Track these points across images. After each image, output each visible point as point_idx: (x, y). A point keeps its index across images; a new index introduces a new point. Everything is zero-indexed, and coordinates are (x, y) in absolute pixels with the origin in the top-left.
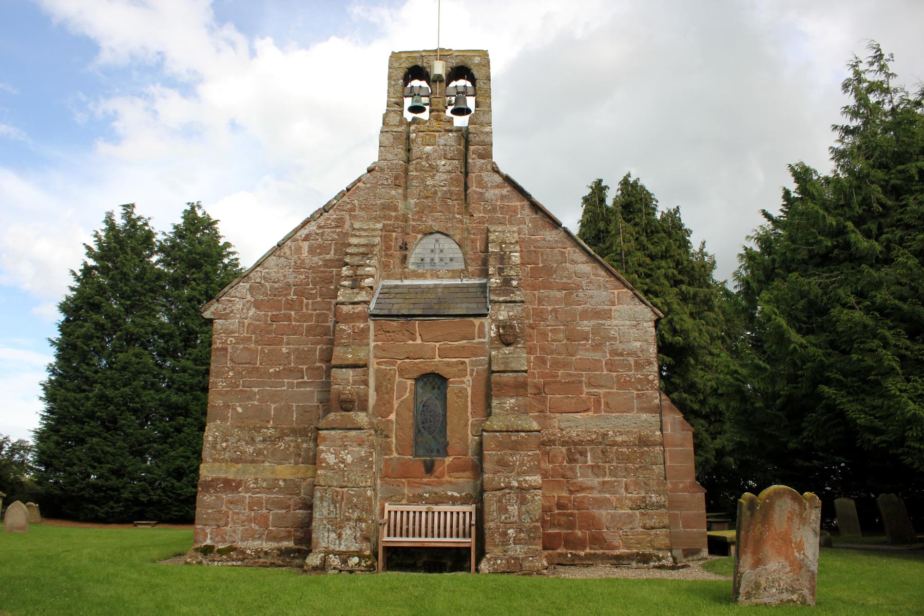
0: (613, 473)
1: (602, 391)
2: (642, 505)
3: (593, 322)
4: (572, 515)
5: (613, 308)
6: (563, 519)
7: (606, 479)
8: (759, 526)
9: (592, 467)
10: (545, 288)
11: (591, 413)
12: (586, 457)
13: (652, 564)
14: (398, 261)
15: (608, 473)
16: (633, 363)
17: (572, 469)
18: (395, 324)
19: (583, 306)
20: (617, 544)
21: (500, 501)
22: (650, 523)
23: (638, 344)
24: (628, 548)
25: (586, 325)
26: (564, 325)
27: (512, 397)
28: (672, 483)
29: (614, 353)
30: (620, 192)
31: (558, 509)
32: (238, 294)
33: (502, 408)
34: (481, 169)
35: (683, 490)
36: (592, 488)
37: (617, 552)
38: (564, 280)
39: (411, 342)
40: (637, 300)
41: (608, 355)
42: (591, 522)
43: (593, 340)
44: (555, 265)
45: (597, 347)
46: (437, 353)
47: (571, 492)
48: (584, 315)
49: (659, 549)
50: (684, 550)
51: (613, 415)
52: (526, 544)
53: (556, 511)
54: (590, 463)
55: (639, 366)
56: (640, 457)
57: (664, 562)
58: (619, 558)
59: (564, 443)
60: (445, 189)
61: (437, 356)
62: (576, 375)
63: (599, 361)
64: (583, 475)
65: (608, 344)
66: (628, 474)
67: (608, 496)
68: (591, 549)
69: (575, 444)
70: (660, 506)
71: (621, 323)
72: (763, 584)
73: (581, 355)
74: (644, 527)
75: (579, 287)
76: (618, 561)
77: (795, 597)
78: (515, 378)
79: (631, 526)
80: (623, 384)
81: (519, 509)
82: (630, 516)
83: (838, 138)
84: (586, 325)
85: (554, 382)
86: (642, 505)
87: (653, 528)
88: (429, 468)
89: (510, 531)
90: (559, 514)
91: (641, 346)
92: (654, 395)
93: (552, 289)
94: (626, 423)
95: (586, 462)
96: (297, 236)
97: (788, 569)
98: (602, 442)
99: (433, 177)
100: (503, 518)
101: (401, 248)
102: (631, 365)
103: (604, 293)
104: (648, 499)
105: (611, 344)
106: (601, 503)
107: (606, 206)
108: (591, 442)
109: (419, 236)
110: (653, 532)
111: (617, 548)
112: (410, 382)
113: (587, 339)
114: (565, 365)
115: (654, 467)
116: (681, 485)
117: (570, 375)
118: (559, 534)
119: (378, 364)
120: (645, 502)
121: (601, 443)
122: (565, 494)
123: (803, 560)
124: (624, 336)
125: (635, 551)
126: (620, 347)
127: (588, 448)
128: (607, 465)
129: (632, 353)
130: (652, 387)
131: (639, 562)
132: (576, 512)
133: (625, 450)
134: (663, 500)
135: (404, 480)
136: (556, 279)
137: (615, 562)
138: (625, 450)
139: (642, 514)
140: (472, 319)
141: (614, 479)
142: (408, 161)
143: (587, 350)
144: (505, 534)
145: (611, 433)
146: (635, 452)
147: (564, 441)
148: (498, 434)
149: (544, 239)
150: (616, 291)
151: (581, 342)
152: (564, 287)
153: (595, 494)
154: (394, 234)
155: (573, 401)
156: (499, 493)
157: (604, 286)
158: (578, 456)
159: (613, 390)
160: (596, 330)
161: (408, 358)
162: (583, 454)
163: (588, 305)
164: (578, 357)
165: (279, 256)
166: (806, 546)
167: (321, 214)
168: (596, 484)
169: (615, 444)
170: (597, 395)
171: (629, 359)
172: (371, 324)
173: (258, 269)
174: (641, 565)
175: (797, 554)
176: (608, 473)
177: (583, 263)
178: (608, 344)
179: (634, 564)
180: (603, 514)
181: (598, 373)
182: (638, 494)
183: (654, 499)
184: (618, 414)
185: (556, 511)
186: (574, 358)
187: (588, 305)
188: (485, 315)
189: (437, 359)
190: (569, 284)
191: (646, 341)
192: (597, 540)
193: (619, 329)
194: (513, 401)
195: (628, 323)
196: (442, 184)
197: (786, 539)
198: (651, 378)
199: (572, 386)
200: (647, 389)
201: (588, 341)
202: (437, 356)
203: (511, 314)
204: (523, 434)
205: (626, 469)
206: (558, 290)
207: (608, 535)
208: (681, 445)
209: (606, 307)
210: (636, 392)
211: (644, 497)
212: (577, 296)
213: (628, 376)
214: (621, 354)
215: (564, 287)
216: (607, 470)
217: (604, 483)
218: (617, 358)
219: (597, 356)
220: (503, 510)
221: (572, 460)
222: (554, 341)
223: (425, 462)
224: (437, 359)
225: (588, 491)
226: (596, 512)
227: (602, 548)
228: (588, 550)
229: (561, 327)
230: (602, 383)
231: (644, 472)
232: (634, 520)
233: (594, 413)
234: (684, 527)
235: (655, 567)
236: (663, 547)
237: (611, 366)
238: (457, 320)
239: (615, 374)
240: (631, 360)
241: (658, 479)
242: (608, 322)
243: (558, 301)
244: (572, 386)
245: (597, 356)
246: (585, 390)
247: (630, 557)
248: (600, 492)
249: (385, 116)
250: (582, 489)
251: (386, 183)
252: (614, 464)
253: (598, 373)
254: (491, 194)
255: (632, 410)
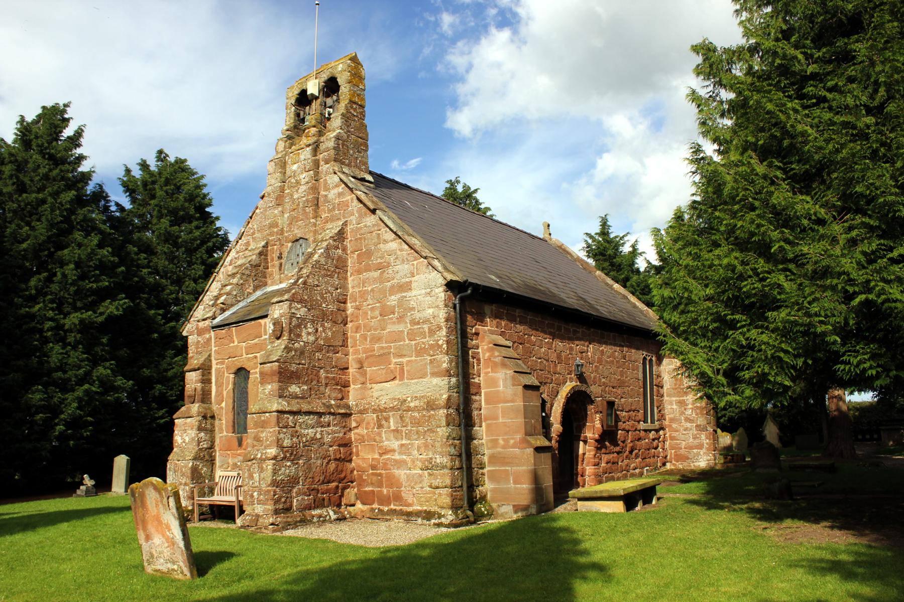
0: (408, 437)
1: (404, 360)
2: (429, 466)
3: (399, 296)
4: (380, 475)
5: (413, 279)
6: (375, 478)
7: (404, 442)
8: (141, 509)
9: (393, 431)
10: (366, 271)
11: (397, 382)
12: (389, 422)
13: (433, 521)
14: (277, 269)
17: (379, 434)
18: (223, 331)
20: (411, 502)
21: (249, 470)
22: (436, 483)
23: (431, 311)
24: (421, 505)
25: (393, 300)
26: (380, 302)
28: (504, 440)
29: (414, 322)
33: (264, 393)
34: (327, 173)
35: (514, 446)
36: (394, 451)
37: (410, 509)
39: (232, 345)
40: (430, 267)
41: (409, 326)
42: (393, 481)
43: (398, 312)
45: (401, 319)
47: (381, 455)
48: (394, 290)
49: (442, 508)
50: (514, 506)
51: (413, 381)
52: (263, 504)
53: (371, 471)
54: (393, 428)
55: (432, 332)
56: (428, 421)
57: (443, 520)
58: (409, 514)
59: (374, 411)
60: (304, 199)
61: (244, 354)
62: (386, 348)
63: (402, 332)
64: (387, 439)
65: (409, 314)
66: (419, 437)
67: (404, 457)
68: (394, 505)
69: (381, 411)
70: (443, 467)
71: (419, 292)
72: (156, 555)
73: (391, 328)
74: (431, 487)
76: (409, 516)
77: (175, 567)
78: (271, 367)
79: (421, 485)
80: (420, 352)
82: (421, 476)
84: (393, 300)
85: (371, 356)
86: (429, 466)
87: (437, 488)
88: (240, 444)
89: (255, 494)
90: (373, 474)
92: (443, 360)
93: (370, 271)
94: (421, 389)
97: (166, 545)
98: (401, 407)
101: (279, 257)
102: (425, 333)
103: (406, 266)
104: (434, 460)
105: (412, 315)
106: (400, 464)
107: (737, 97)
110: (437, 491)
112: (232, 376)
113: (393, 313)
114: (379, 339)
115: (438, 430)
116: (512, 442)
117: (382, 348)
118: (373, 491)
120: (431, 463)
122: (377, 456)
123: (173, 538)
124: (420, 305)
125: (425, 508)
126: (417, 316)
127: (391, 414)
128: (404, 429)
129: (427, 321)
130: (441, 352)
131: (423, 519)
132: (383, 472)
133: (416, 414)
134: (445, 461)
135: (229, 452)
136: (375, 261)
137: (406, 518)
138: (416, 414)
139: (430, 475)
140: (260, 321)
141: (409, 442)
143: (394, 323)
144: (252, 496)
145: (409, 399)
146: (424, 416)
147: (374, 409)
148: (254, 415)
149: (365, 226)
150: (415, 263)
151: (390, 316)
152: (379, 267)
153: (397, 457)
154: (275, 247)
155: (384, 372)
156: (250, 463)
158: (384, 422)
159: (413, 358)
160: (401, 302)
161: (229, 358)
162: (387, 419)
163: (396, 281)
164: (388, 330)
166: (172, 527)
167: (237, 242)
168: (396, 448)
169: (409, 409)
170: (401, 364)
171: (424, 326)
172: (212, 333)
174: (425, 521)
175: (168, 533)
177: (392, 241)
178: (409, 314)
179: (420, 521)
180: (401, 474)
181: (402, 343)
182: (427, 455)
183: (438, 461)
184: (416, 381)
185: (371, 471)
187: (396, 281)
188: (266, 316)
189: (245, 356)
190: (382, 263)
191: (437, 307)
192: (398, 498)
193: (417, 299)
195: (423, 291)
197: (158, 519)
198: (440, 342)
199: (383, 358)
200: (438, 354)
202: (244, 354)
203: (281, 311)
204: (267, 414)
205: (417, 432)
206: (375, 270)
207: (407, 496)
208: (512, 401)
209: (407, 280)
210: (429, 358)
211: (431, 459)
213: (423, 343)
214: (418, 323)
215: (379, 267)
216: (404, 434)
217: (402, 445)
218: (416, 327)
219: (401, 327)
221: (380, 426)
222: (372, 318)
223: (238, 437)
224: (245, 356)
225: (392, 453)
226: (396, 472)
227: (401, 505)
228: (392, 507)
229: (377, 305)
230: (404, 353)
231: (431, 435)
232: (423, 480)
233: (400, 381)
234: (515, 482)
235: (435, 524)
236: (445, 505)
237: (412, 336)
238: (253, 322)
239: (413, 342)
240: (426, 327)
241: (442, 441)
242: (408, 294)
243: (375, 280)
244: (383, 358)
245: (401, 327)
247: (418, 514)
248: (400, 453)
250: (387, 452)
252: (409, 428)
254: (332, 194)
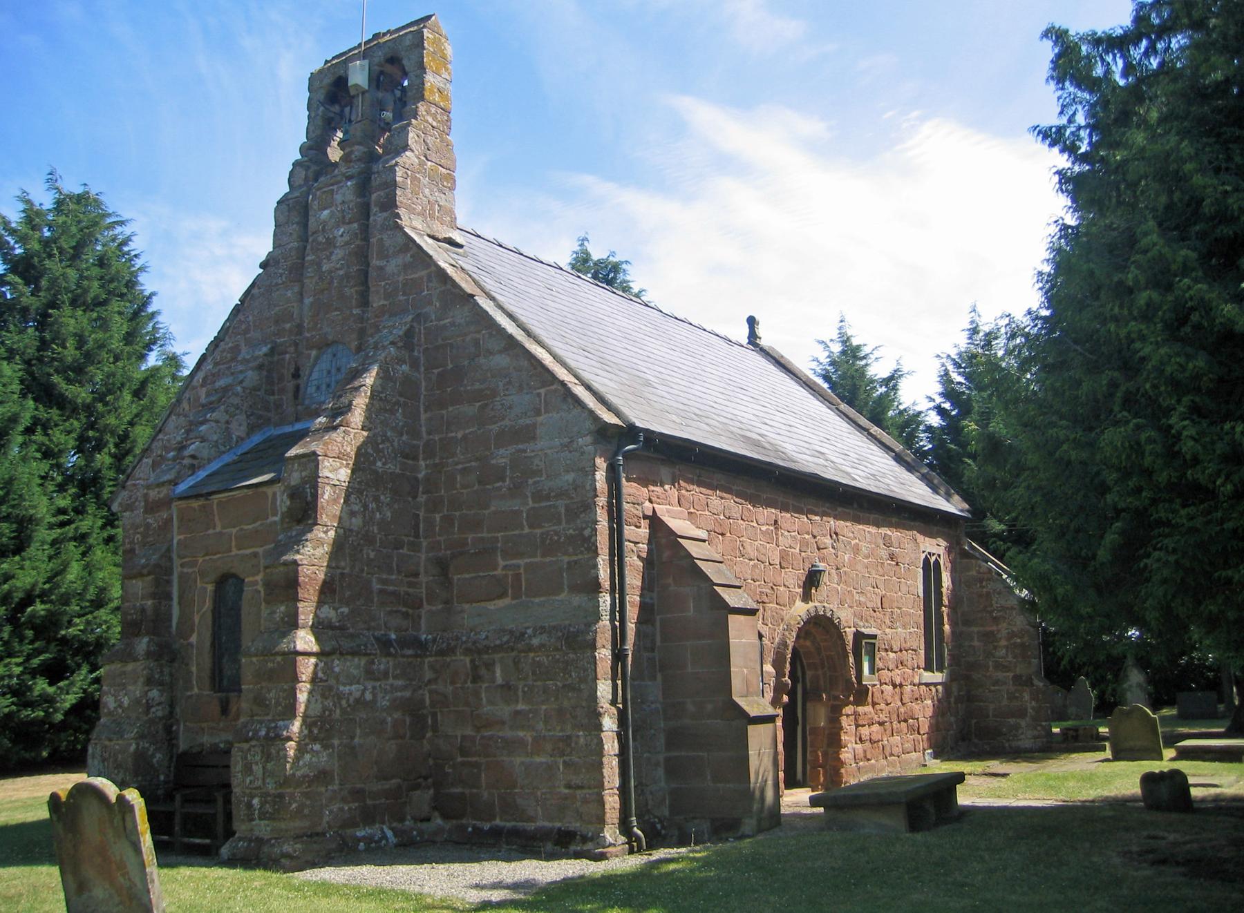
1: (521, 562)
3: (511, 449)
5: (540, 419)
12: (494, 672)
15: (521, 698)
16: (563, 510)
17: (477, 694)
19: (499, 424)
22: (576, 780)
25: (502, 457)
27: (282, 602)
29: (538, 496)
30: (1120, 32)
31: (462, 756)
32: (142, 475)
37: (531, 826)
38: (477, 386)
41: (530, 502)
44: (466, 363)
46: (233, 543)
59: (468, 651)
60: (341, 272)
64: (490, 702)
65: (530, 481)
69: (479, 652)
75: (495, 393)
81: (264, 768)
83: (144, 274)
87: (581, 788)
91: (574, 481)
95: (493, 680)
96: (195, 383)
99: (328, 258)
100: (248, 781)
103: (527, 398)
108: (499, 648)
109: (314, 353)
111: (531, 819)
116: (710, 707)
119: (182, 565)
121: (513, 649)
122: (469, 732)
127: (497, 656)
129: (562, 494)
140: (264, 489)
142: (304, 239)
150: (542, 391)
157: (528, 384)
162: (490, 666)
163: (507, 422)
165: (179, 415)
173: (160, 436)
176: (521, 698)
181: (517, 532)
185: (459, 759)
186: (486, 512)
187: (507, 422)
194: (283, 608)
196: (338, 266)
201: (504, 481)
209: (528, 422)
212: (492, 409)
213: (557, 533)
217: (517, 713)
219: (515, 505)
220: (248, 769)
233: (513, 598)
245: (515, 505)
246: (502, 563)
249: (291, 173)
250: (489, 725)
251: (280, 282)
253: (517, 532)
255: (507, 596)
